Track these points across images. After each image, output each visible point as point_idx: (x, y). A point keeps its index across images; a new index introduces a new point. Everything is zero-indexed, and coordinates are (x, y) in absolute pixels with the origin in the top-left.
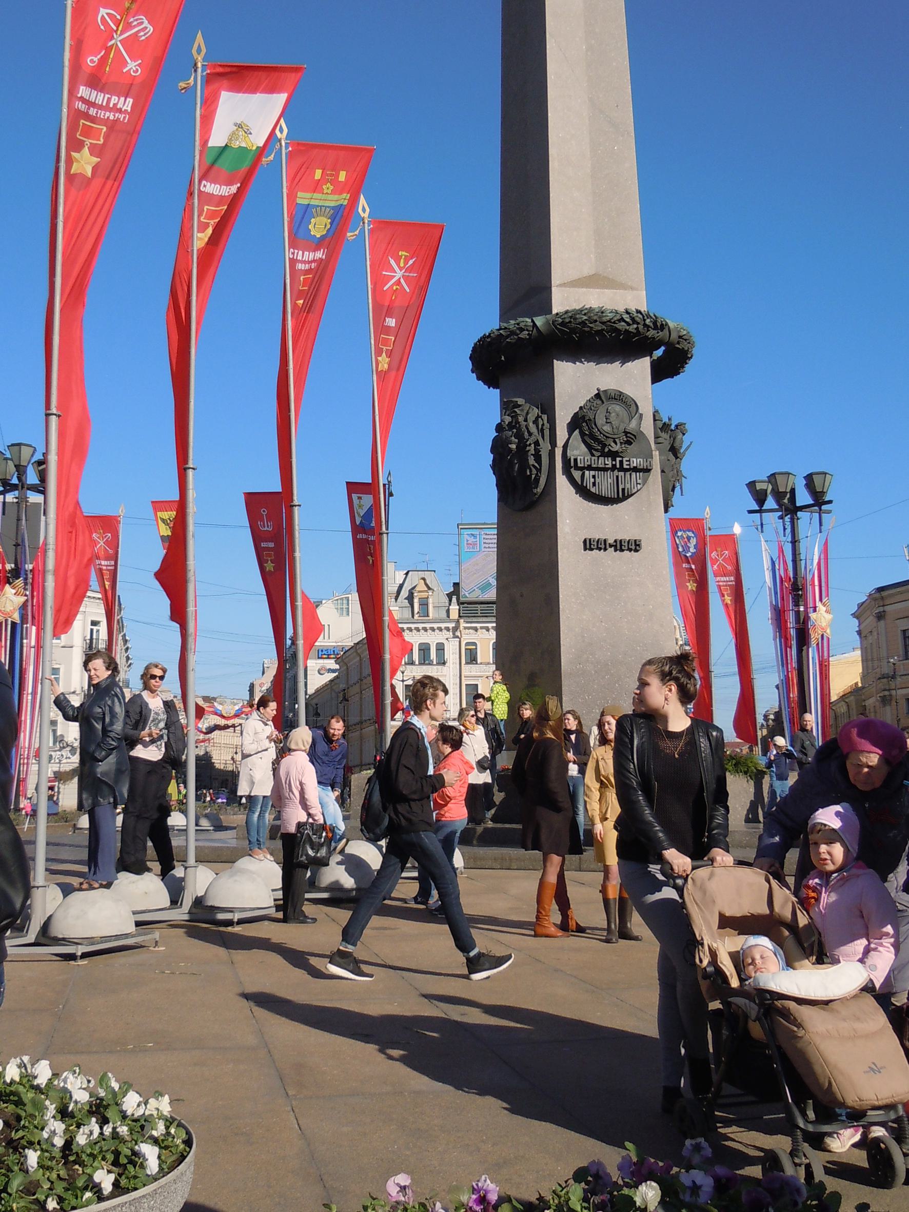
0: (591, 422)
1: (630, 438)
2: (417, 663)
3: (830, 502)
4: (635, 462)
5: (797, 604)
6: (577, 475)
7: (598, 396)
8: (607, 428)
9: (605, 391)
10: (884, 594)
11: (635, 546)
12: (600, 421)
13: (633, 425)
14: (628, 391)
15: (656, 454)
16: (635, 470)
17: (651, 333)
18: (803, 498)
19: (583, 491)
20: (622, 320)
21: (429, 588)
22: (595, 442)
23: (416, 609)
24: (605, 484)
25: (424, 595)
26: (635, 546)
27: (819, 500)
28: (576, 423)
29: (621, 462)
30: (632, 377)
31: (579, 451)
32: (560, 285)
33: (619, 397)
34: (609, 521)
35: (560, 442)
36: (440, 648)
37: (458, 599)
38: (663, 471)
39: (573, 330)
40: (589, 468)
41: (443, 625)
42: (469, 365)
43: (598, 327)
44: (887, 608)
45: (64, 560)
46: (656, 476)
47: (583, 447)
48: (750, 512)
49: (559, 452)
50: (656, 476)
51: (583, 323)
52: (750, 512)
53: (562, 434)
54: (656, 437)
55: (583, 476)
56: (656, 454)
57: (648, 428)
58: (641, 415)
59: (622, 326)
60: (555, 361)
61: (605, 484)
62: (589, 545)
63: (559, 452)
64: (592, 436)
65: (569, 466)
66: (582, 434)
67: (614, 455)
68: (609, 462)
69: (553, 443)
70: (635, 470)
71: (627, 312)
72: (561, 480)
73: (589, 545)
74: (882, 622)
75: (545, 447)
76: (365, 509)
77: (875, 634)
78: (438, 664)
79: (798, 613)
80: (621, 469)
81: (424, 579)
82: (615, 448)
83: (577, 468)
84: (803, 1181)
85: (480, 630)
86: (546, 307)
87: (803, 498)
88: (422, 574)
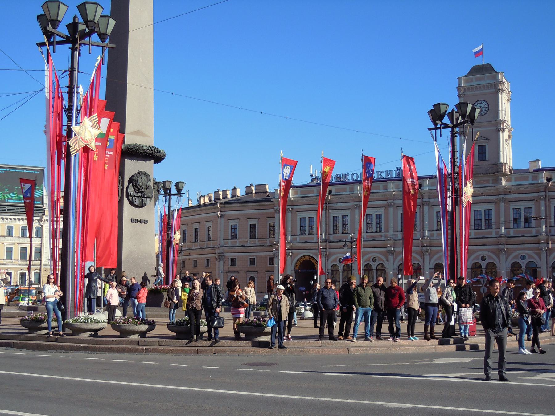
0: (136, 181)
1: (147, 187)
3: (184, 194)
4: (148, 195)
5: (168, 231)
6: (130, 198)
7: (139, 173)
11: (146, 222)
12: (139, 181)
16: (148, 198)
17: (156, 154)
18: (174, 191)
19: (132, 203)
20: (148, 149)
22: (137, 188)
24: (138, 201)
26: (146, 222)
27: (179, 192)
28: (131, 180)
30: (147, 166)
31: (131, 190)
33: (145, 174)
34: (139, 213)
35: (125, 186)
39: (133, 151)
40: (135, 196)
43: (141, 151)
45: (429, 331)
47: (133, 189)
49: (125, 189)
50: (153, 199)
51: (137, 149)
53: (126, 184)
55: (132, 198)
57: (151, 184)
59: (148, 151)
61: (138, 201)
62: (132, 221)
63: (125, 189)
64: (136, 186)
65: (128, 194)
66: (133, 185)
67: (142, 192)
68: (140, 195)
69: (123, 187)
70: (148, 198)
72: (125, 199)
73: (132, 221)
76: (26, 189)
79: (168, 234)
80: (144, 197)
82: (143, 190)
83: (131, 196)
84: (506, 86)
87: (174, 191)
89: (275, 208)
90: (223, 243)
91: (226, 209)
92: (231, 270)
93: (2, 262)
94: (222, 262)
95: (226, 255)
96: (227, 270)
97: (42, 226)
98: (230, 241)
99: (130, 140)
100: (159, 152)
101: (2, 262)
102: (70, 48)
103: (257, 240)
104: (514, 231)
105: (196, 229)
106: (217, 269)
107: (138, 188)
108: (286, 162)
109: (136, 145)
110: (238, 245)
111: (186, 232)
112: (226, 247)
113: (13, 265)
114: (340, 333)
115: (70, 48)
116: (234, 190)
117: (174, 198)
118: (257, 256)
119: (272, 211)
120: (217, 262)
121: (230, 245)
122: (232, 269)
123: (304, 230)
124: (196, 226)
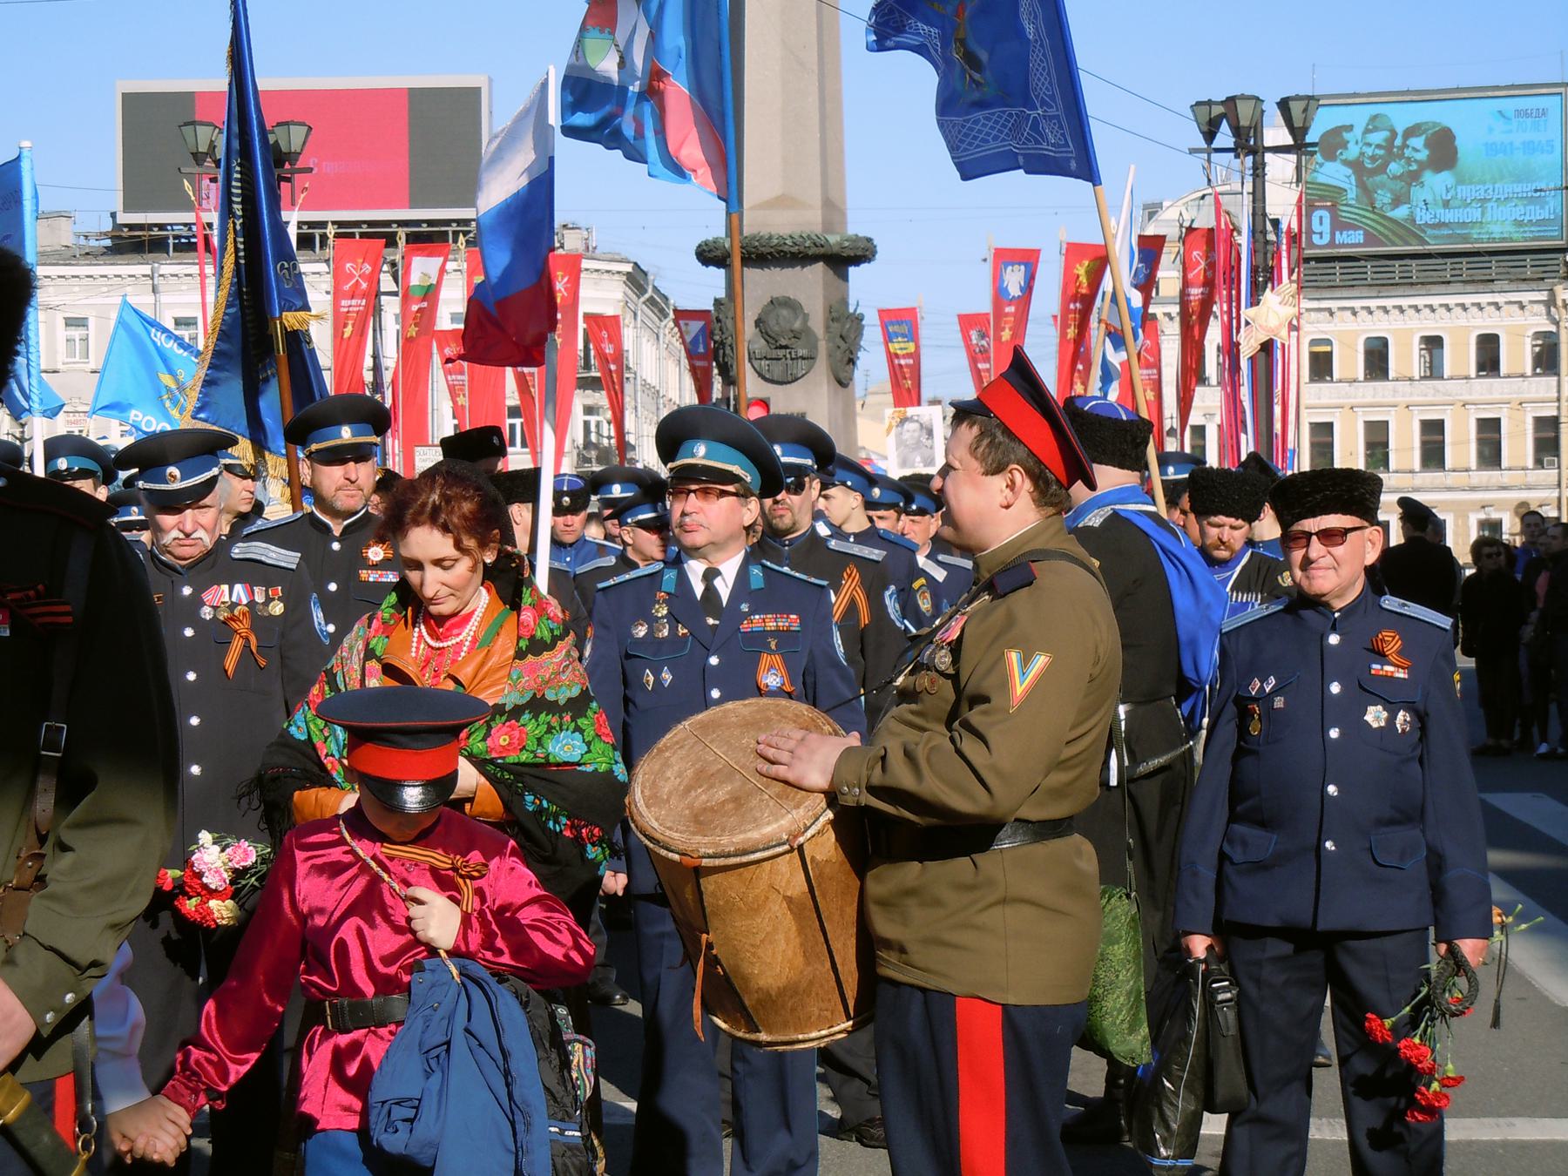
13: (797, 325)
15: (823, 347)
31: (760, 345)
32: (752, 208)
46: (821, 366)
48: (1193, 151)
52: (1193, 151)
54: (827, 328)
57: (817, 324)
61: (777, 370)
67: (786, 347)
68: (781, 353)
82: (783, 342)
97: (1557, 323)
108: (1004, 257)
113: (1449, 489)
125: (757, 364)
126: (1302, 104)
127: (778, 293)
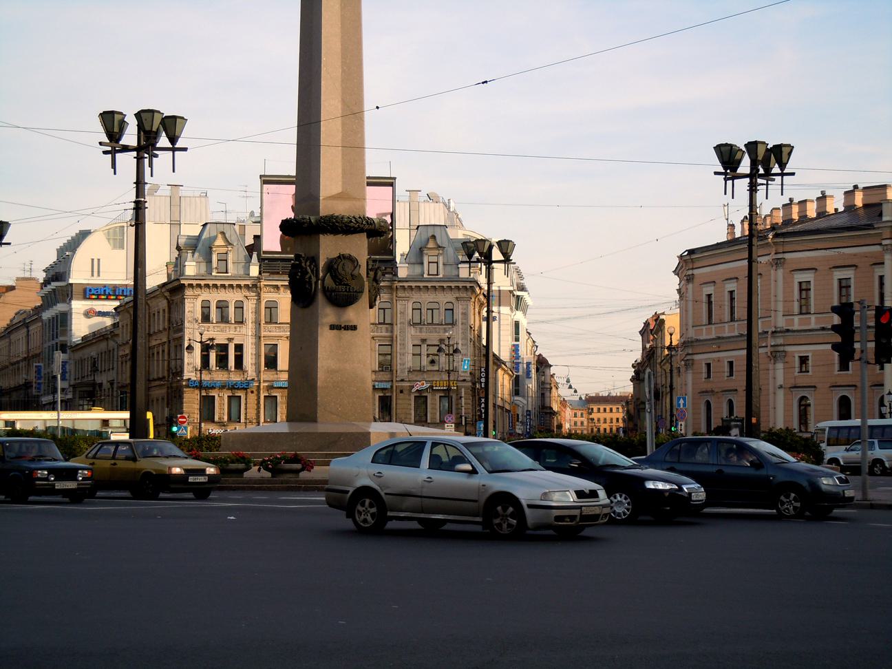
2: (214, 322)
6: (328, 294)
7: (339, 257)
8: (343, 273)
9: (343, 255)
10: (694, 256)
14: (353, 254)
15: (366, 283)
20: (351, 222)
21: (230, 244)
22: (335, 277)
23: (215, 264)
25: (223, 250)
27: (507, 260)
29: (349, 288)
31: (329, 282)
36: (239, 307)
37: (259, 256)
38: (369, 291)
41: (242, 283)
42: (284, 219)
44: (696, 272)
54: (368, 274)
56: (366, 283)
58: (360, 266)
60: (321, 236)
65: (326, 291)
66: (331, 275)
71: (354, 217)
74: (690, 286)
75: (314, 279)
77: (430, 368)
78: (236, 322)
81: (223, 233)
85: (282, 289)
86: (318, 212)
87: (497, 255)
88: (221, 228)
89: (884, 242)
90: (781, 323)
91: (787, 248)
92: (800, 382)
93: (883, 491)
94: (780, 366)
95: (788, 349)
96: (791, 382)
98: (796, 319)
99: (326, 208)
100: (436, 194)
101: (883, 491)
102: (135, 158)
103: (813, 318)
104: (810, 324)
105: (731, 292)
106: (771, 380)
107: (339, 279)
109: (332, 216)
110: (813, 326)
111: (736, 295)
112: (788, 331)
114: (230, 419)
115: (135, 158)
116: (823, 198)
117: (498, 269)
118: (814, 351)
119: (878, 248)
120: (771, 366)
121: (796, 327)
122: (803, 380)
123: (808, 305)
124: (709, 289)
125: (328, 294)
126: (789, 149)
127: (347, 252)
